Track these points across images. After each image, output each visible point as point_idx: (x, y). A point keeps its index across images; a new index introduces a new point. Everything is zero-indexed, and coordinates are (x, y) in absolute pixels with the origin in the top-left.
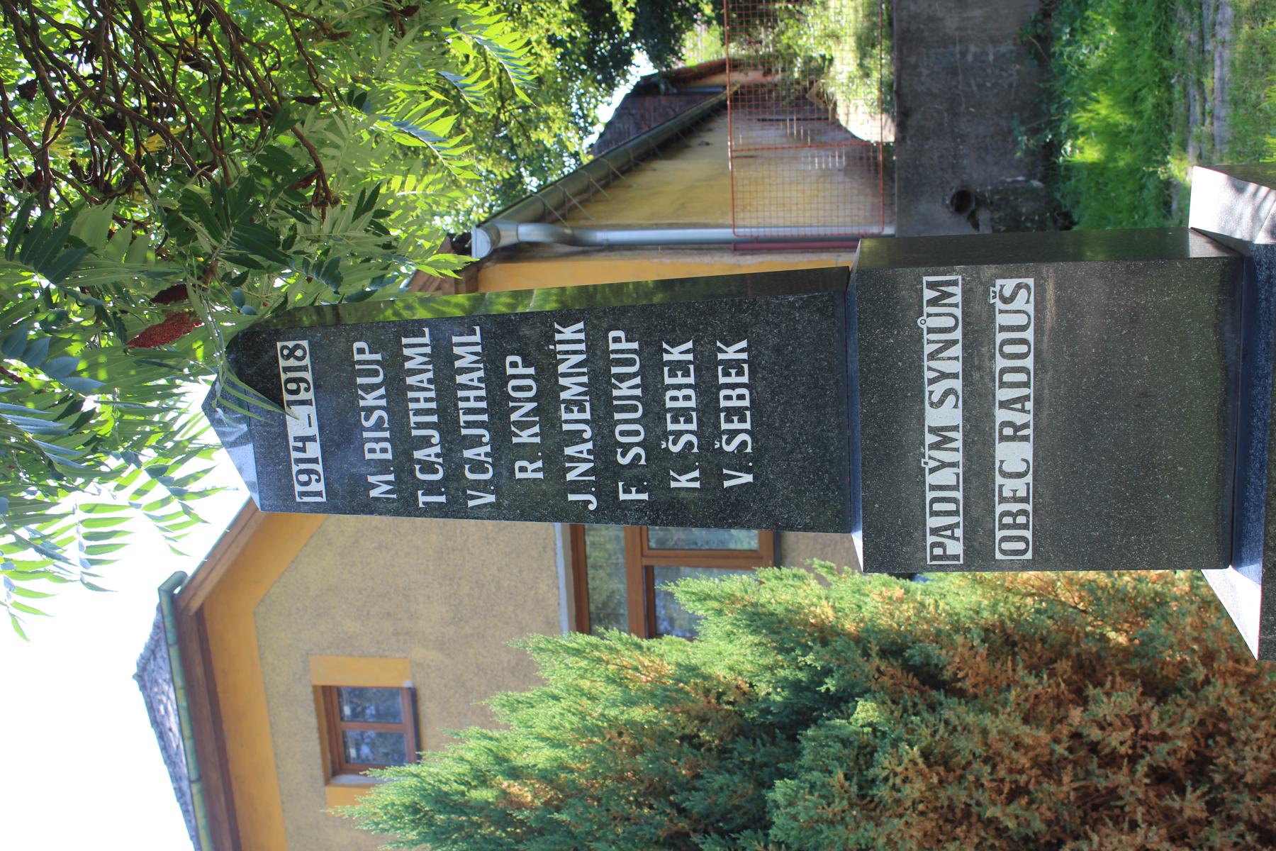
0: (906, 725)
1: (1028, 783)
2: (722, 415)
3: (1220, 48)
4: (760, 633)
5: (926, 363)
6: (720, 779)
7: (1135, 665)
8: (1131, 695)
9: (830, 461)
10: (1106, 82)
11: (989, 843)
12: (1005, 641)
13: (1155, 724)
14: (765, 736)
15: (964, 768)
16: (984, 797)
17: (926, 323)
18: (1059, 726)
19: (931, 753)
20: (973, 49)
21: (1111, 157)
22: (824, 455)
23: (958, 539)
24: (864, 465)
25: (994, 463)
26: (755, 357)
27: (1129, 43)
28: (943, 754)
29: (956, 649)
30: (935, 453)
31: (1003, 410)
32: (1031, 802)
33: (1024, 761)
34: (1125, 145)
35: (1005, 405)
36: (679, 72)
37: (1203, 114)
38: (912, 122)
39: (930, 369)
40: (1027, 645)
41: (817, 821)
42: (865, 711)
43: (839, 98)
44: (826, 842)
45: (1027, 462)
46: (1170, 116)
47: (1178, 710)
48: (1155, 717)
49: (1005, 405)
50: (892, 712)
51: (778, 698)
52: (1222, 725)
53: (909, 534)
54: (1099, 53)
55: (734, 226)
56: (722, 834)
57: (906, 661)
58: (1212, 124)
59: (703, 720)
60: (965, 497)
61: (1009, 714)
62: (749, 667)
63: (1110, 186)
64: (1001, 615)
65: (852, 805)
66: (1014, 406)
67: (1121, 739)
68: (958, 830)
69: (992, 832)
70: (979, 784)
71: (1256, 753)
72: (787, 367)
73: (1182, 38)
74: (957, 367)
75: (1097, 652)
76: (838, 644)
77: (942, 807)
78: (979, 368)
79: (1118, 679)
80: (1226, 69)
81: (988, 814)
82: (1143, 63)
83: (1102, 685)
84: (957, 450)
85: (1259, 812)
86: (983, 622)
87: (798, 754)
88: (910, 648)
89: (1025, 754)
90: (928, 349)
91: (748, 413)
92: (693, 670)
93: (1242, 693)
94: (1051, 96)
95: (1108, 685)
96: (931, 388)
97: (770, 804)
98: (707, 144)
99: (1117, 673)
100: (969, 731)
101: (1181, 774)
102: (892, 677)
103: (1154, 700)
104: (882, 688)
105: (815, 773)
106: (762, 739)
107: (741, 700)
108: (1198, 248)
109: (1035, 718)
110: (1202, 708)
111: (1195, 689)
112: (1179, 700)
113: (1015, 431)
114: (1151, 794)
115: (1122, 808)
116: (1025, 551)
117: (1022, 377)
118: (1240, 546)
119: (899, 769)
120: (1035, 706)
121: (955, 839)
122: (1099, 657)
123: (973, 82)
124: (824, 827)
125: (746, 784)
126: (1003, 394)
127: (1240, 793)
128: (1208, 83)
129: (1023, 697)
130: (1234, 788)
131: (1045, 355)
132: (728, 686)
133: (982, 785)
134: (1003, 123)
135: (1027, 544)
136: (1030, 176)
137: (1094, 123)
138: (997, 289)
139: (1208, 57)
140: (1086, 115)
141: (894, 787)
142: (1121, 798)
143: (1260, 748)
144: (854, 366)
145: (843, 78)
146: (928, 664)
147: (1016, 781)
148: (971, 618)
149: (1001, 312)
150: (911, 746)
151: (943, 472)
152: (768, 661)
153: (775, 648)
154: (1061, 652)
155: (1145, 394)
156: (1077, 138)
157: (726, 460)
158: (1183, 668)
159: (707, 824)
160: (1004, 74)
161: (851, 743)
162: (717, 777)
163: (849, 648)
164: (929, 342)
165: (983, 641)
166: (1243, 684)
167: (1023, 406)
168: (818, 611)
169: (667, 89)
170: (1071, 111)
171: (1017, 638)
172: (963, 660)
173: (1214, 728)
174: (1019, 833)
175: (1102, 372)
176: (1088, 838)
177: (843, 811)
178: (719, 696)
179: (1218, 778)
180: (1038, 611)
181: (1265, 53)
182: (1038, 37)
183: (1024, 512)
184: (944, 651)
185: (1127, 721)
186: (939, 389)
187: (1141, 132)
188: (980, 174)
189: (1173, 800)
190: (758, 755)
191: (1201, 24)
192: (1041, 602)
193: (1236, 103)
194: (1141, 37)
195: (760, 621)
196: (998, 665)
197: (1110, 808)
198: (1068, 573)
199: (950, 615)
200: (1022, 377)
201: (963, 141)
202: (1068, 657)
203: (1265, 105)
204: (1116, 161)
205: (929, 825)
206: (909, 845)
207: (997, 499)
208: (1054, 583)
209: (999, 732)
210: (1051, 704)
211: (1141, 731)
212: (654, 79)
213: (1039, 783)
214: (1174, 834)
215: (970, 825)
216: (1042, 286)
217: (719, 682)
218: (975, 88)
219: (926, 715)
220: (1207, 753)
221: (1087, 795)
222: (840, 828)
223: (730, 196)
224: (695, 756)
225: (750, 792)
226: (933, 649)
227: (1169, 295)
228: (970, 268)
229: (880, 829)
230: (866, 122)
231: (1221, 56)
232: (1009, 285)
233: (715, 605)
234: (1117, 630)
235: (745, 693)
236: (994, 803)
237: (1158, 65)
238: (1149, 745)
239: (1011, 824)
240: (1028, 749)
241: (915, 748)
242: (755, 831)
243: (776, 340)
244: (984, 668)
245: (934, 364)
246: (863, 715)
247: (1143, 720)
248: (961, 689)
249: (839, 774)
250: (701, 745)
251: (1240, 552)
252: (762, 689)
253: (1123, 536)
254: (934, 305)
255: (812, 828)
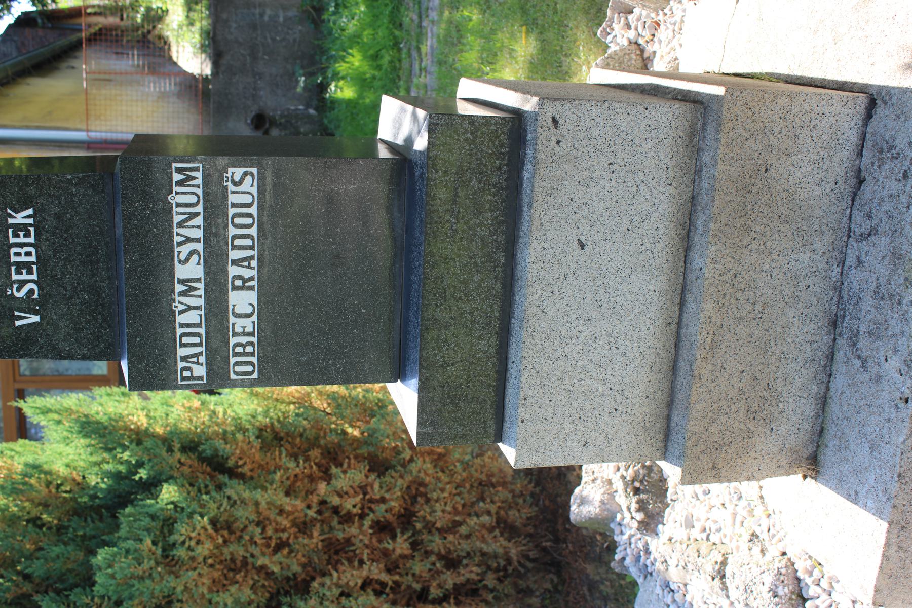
0: (199, 501)
1: (288, 538)
2: (13, 268)
3: (431, 25)
4: (90, 437)
5: (175, 230)
6: (57, 550)
7: (364, 451)
8: (361, 472)
9: (103, 305)
10: (358, 43)
11: (260, 584)
12: (273, 437)
13: (376, 491)
14: (94, 516)
15: (242, 531)
16: (256, 551)
17: (175, 199)
18: (310, 496)
19: (218, 521)
20: (268, 12)
21: (361, 96)
22: (98, 300)
23: (202, 364)
24: (127, 308)
25: (228, 307)
26: (40, 222)
27: (374, 16)
28: (227, 522)
29: (237, 444)
30: (183, 299)
31: (234, 267)
32: (291, 552)
33: (285, 522)
34: (371, 87)
35: (235, 263)
36: (54, 12)
37: (420, 70)
38: (225, 60)
39: (178, 234)
40: (290, 439)
41: (131, 578)
42: (169, 493)
43: (172, 40)
44: (138, 593)
45: (253, 306)
46: (400, 69)
47: (393, 481)
48: (376, 486)
49: (235, 263)
50: (189, 493)
51: (103, 486)
52: (421, 489)
53: (163, 360)
54: (354, 22)
55: (88, 131)
56: (58, 592)
57: (200, 454)
58: (425, 76)
59: (46, 505)
60: (206, 333)
61: (275, 490)
62: (82, 464)
63: (360, 115)
64: (271, 418)
65: (157, 564)
66: (242, 264)
67: (354, 503)
68: (238, 576)
69: (263, 575)
70: (253, 542)
71: (443, 507)
72: (66, 231)
73: (409, 17)
74: (199, 233)
75: (339, 442)
76: (148, 443)
77: (226, 560)
78: (216, 235)
79: (353, 461)
80: (434, 40)
81: (259, 563)
82: (381, 33)
83: (341, 465)
84: (200, 296)
85: (445, 547)
86: (258, 423)
87: (117, 527)
88: (203, 444)
89: (287, 517)
90: (177, 219)
91: (35, 267)
92: (36, 467)
93: (435, 467)
94: (323, 51)
95: (345, 465)
96: (179, 249)
97: (95, 567)
98: (73, 68)
99: (351, 456)
100: (245, 504)
101: (395, 525)
102: (190, 466)
103: (376, 474)
104: (183, 475)
105: (129, 541)
106: (92, 517)
107: (76, 489)
108: (383, 153)
109: (295, 491)
110: (409, 478)
111: (404, 466)
112: (394, 474)
113: (244, 283)
114: (374, 540)
115: (354, 551)
116: (253, 372)
117: (248, 242)
118: (405, 366)
119: (193, 535)
120: (295, 482)
121: (237, 582)
122: (340, 446)
123: (268, 35)
124: (135, 582)
125: (78, 553)
126: (234, 255)
127: (432, 535)
128: (424, 49)
129: (285, 477)
130: (430, 532)
131: (265, 226)
132: (65, 479)
133: (256, 543)
134: (289, 67)
135: (254, 367)
136: (308, 106)
137: (350, 71)
138: (229, 175)
139: (424, 31)
140: (345, 65)
141: (190, 549)
142: (354, 545)
143: (446, 504)
144: (119, 231)
145: (175, 26)
146: (217, 456)
147: (280, 538)
148: (249, 421)
149: (232, 192)
150: (202, 516)
151: (189, 313)
152: (94, 459)
153: (101, 448)
154: (314, 443)
155: (338, 257)
156: (339, 81)
157: (17, 304)
158: (397, 451)
159: (46, 585)
160: (290, 32)
161: (158, 517)
162: (54, 548)
163: (157, 446)
164: (177, 214)
165: (258, 437)
166: (436, 460)
167: (249, 264)
168: (135, 419)
169: (43, 23)
170: (335, 62)
171: (282, 434)
172: (242, 451)
173: (417, 493)
174: (281, 575)
175: (307, 240)
176: (331, 575)
177: (151, 569)
178: (58, 486)
179: (419, 526)
180: (297, 415)
181: (458, 31)
182: (314, 7)
183: (251, 344)
184: (228, 446)
185: (358, 490)
186: (185, 250)
187: (380, 79)
188: (272, 102)
189: (388, 543)
190: (88, 529)
191: (420, 7)
192: (299, 408)
193: (440, 63)
194: (381, 13)
195: (89, 427)
196: (268, 454)
197: (346, 553)
198: (319, 387)
199: (233, 418)
200: (248, 242)
201: (260, 78)
202: (319, 446)
203: (457, 65)
204: (363, 98)
205: (216, 574)
206: (200, 590)
207: (230, 334)
208: (308, 394)
209: (268, 503)
210: (306, 481)
211: (368, 497)
212: (32, 15)
213: (296, 537)
214: (391, 567)
215: (247, 571)
216: (263, 174)
217: (59, 476)
218: (269, 40)
219: (214, 494)
220: (412, 509)
221: (331, 544)
222: (148, 582)
223: (84, 107)
224: (38, 534)
225: (81, 558)
226: (219, 444)
227: (354, 184)
228: (208, 158)
229: (178, 580)
230: (191, 59)
231: (432, 31)
232: (238, 172)
233: (56, 417)
234: (352, 426)
235: (78, 484)
236: (263, 554)
237: (392, 34)
238: (373, 506)
239: (276, 569)
240: (289, 514)
241: (206, 518)
242: (84, 589)
243: (57, 209)
244: (258, 457)
245: (181, 231)
246: (167, 496)
247: (369, 489)
248: (241, 473)
249: (148, 541)
250: (43, 525)
251: (405, 370)
252: (93, 480)
253: (324, 360)
254: (181, 186)
255: (126, 584)
